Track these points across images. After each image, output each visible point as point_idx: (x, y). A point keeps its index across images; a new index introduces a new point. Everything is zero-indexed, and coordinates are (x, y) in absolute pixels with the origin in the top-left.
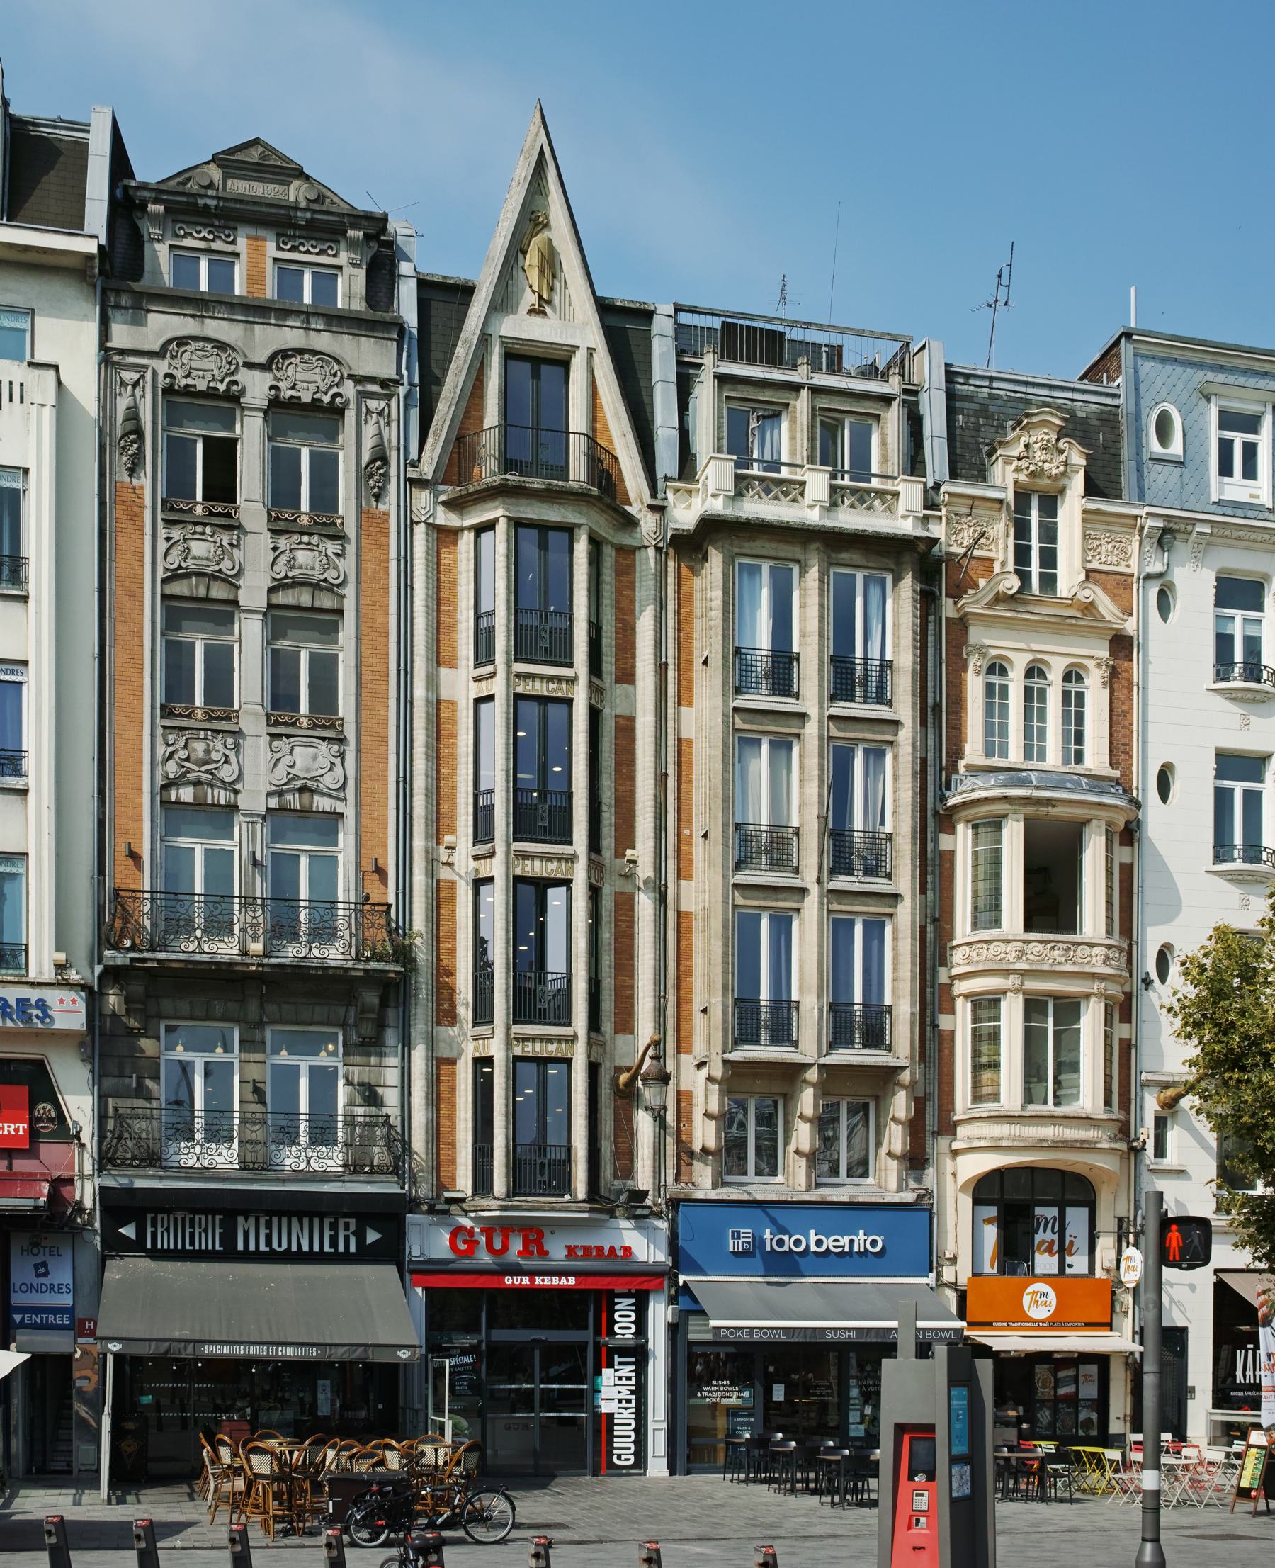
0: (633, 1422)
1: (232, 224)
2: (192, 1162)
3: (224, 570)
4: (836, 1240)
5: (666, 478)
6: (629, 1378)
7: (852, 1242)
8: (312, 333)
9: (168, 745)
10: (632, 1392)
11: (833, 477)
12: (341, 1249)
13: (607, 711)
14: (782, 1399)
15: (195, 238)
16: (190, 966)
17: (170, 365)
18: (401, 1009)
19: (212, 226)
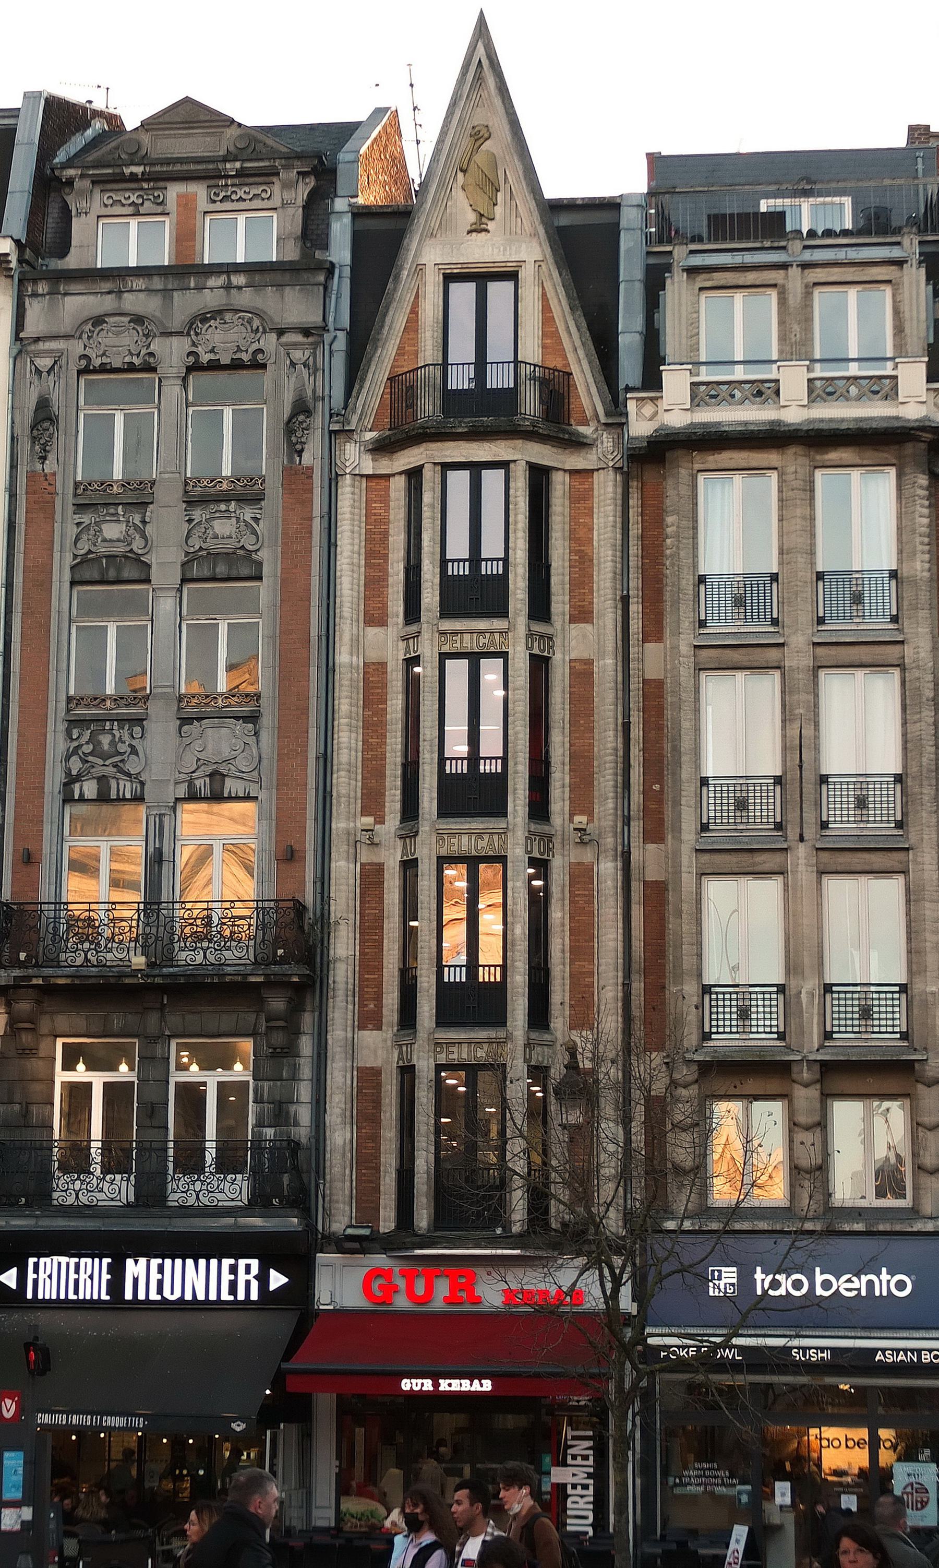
0: (591, 1514)
1: (161, 184)
2: (71, 1200)
3: (135, 549)
4: (849, 1281)
5: (628, 389)
6: (585, 1458)
7: (870, 1284)
8: (234, 291)
9: (72, 740)
10: (589, 1476)
11: (809, 369)
12: (241, 1296)
13: (558, 658)
14: (357, 1430)
15: (123, 205)
16: (77, 982)
17: (85, 346)
18: (317, 1014)
19: (142, 189)
